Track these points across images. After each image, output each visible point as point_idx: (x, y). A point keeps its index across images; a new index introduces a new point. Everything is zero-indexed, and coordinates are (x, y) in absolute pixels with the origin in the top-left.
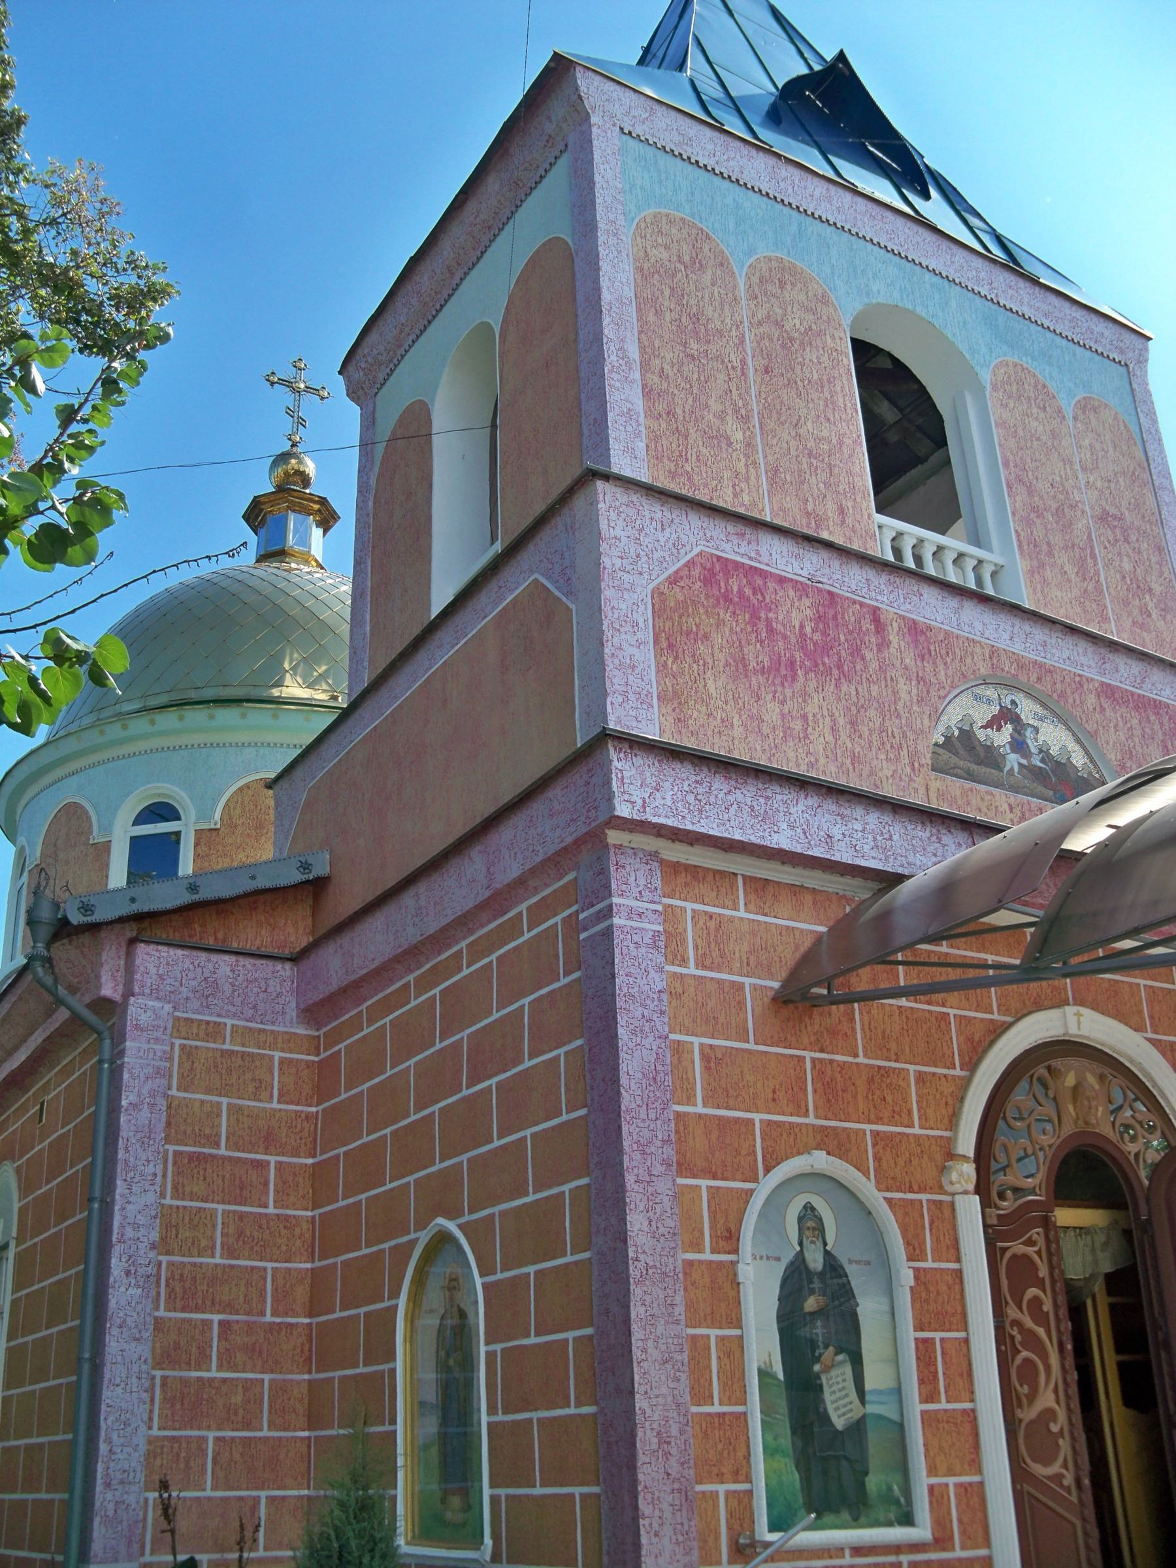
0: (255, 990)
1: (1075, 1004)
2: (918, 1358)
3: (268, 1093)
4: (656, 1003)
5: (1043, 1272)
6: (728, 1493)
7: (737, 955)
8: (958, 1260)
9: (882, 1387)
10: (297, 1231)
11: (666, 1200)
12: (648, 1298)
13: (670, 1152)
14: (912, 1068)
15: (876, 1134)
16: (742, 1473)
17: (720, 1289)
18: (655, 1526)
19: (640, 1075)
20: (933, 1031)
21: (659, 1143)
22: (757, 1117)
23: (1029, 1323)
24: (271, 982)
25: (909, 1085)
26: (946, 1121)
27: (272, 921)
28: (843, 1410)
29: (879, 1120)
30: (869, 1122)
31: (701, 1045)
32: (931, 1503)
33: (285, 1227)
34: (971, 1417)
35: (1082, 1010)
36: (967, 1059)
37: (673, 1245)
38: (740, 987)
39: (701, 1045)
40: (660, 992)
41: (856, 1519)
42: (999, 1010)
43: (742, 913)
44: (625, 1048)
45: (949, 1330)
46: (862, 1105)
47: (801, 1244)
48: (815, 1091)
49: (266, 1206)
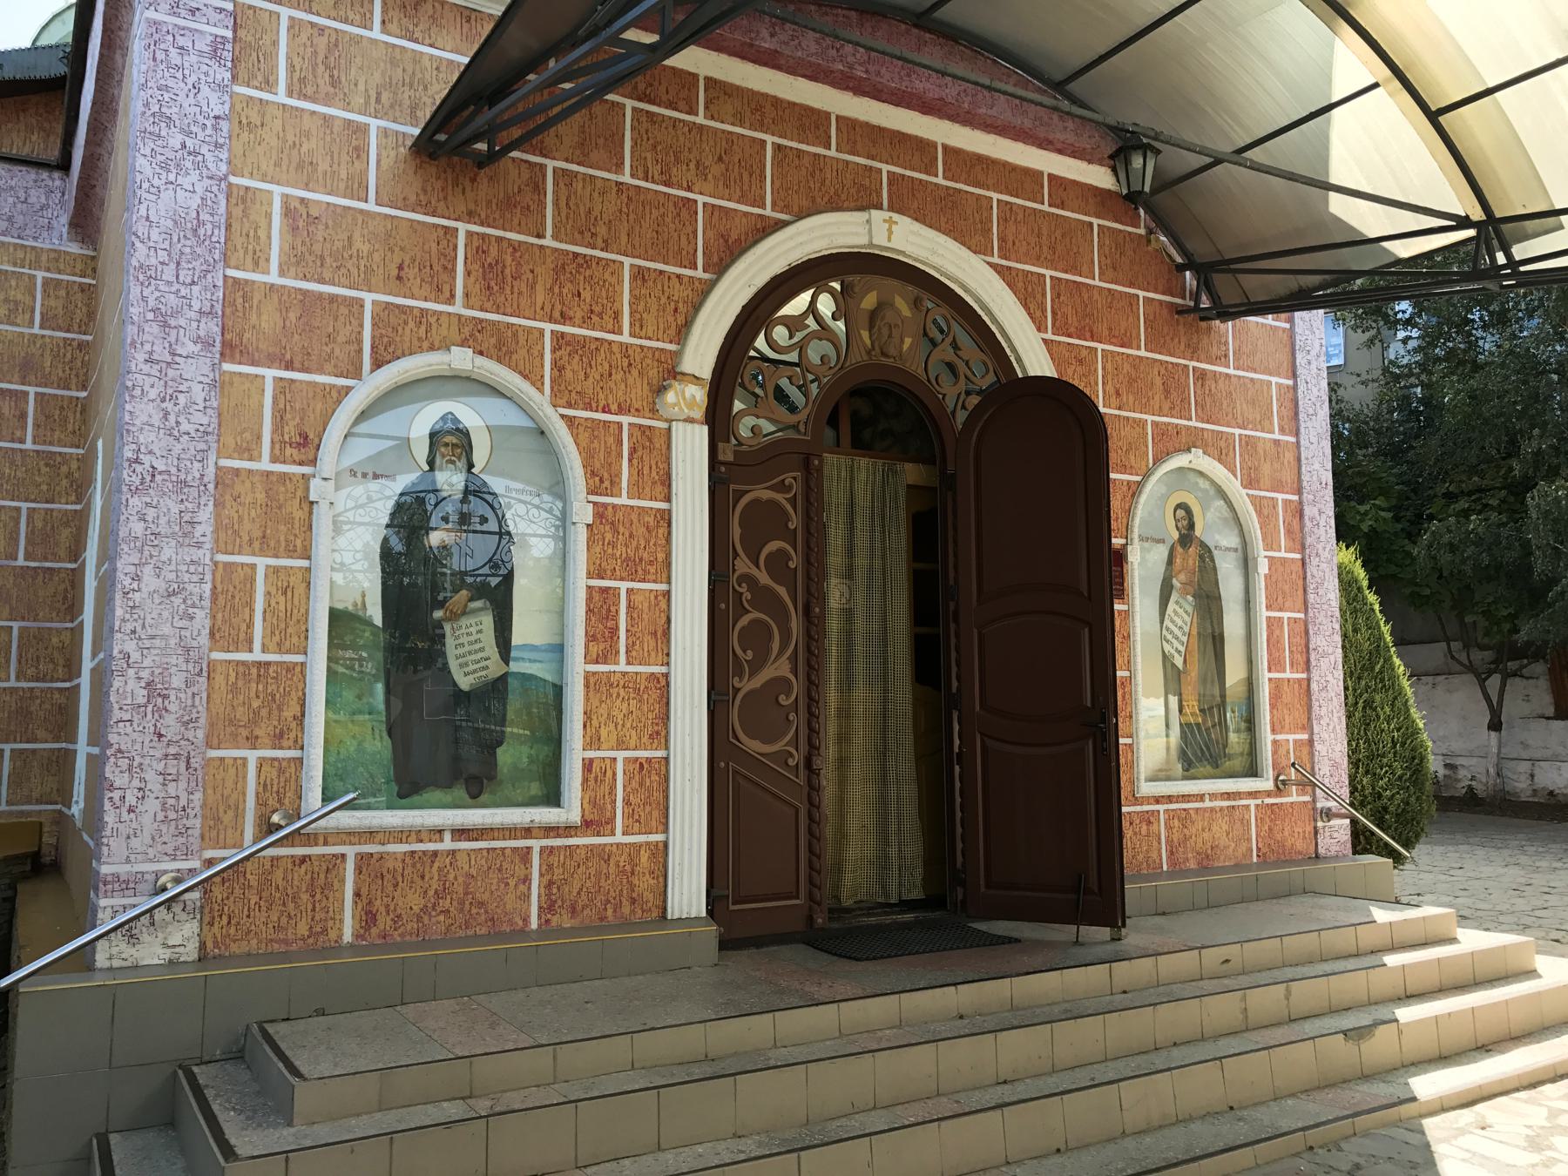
0: (11, 200)
1: (891, 208)
2: (589, 611)
3: (27, 316)
4: (209, 131)
5: (795, 522)
6: (261, 762)
7: (361, 87)
8: (668, 499)
9: (537, 641)
10: (64, 469)
11: (197, 388)
12: (151, 513)
13: (212, 327)
14: (627, 261)
15: (559, 338)
16: (290, 732)
17: (280, 508)
18: (131, 799)
19: (170, 223)
20: (668, 220)
21: (193, 315)
22: (368, 298)
23: (764, 578)
24: (32, 192)
25: (620, 282)
26: (672, 332)
27: (46, 125)
28: (472, 667)
29: (565, 318)
30: (551, 320)
31: (285, 197)
32: (585, 781)
33: (47, 465)
34: (662, 685)
35: (896, 217)
36: (715, 259)
37: (202, 446)
38: (363, 130)
39: (285, 197)
40: (216, 117)
41: (474, 796)
42: (774, 204)
43: (376, 33)
44: (146, 185)
45: (644, 581)
46: (540, 297)
47: (431, 463)
48: (468, 273)
49: (22, 441)
